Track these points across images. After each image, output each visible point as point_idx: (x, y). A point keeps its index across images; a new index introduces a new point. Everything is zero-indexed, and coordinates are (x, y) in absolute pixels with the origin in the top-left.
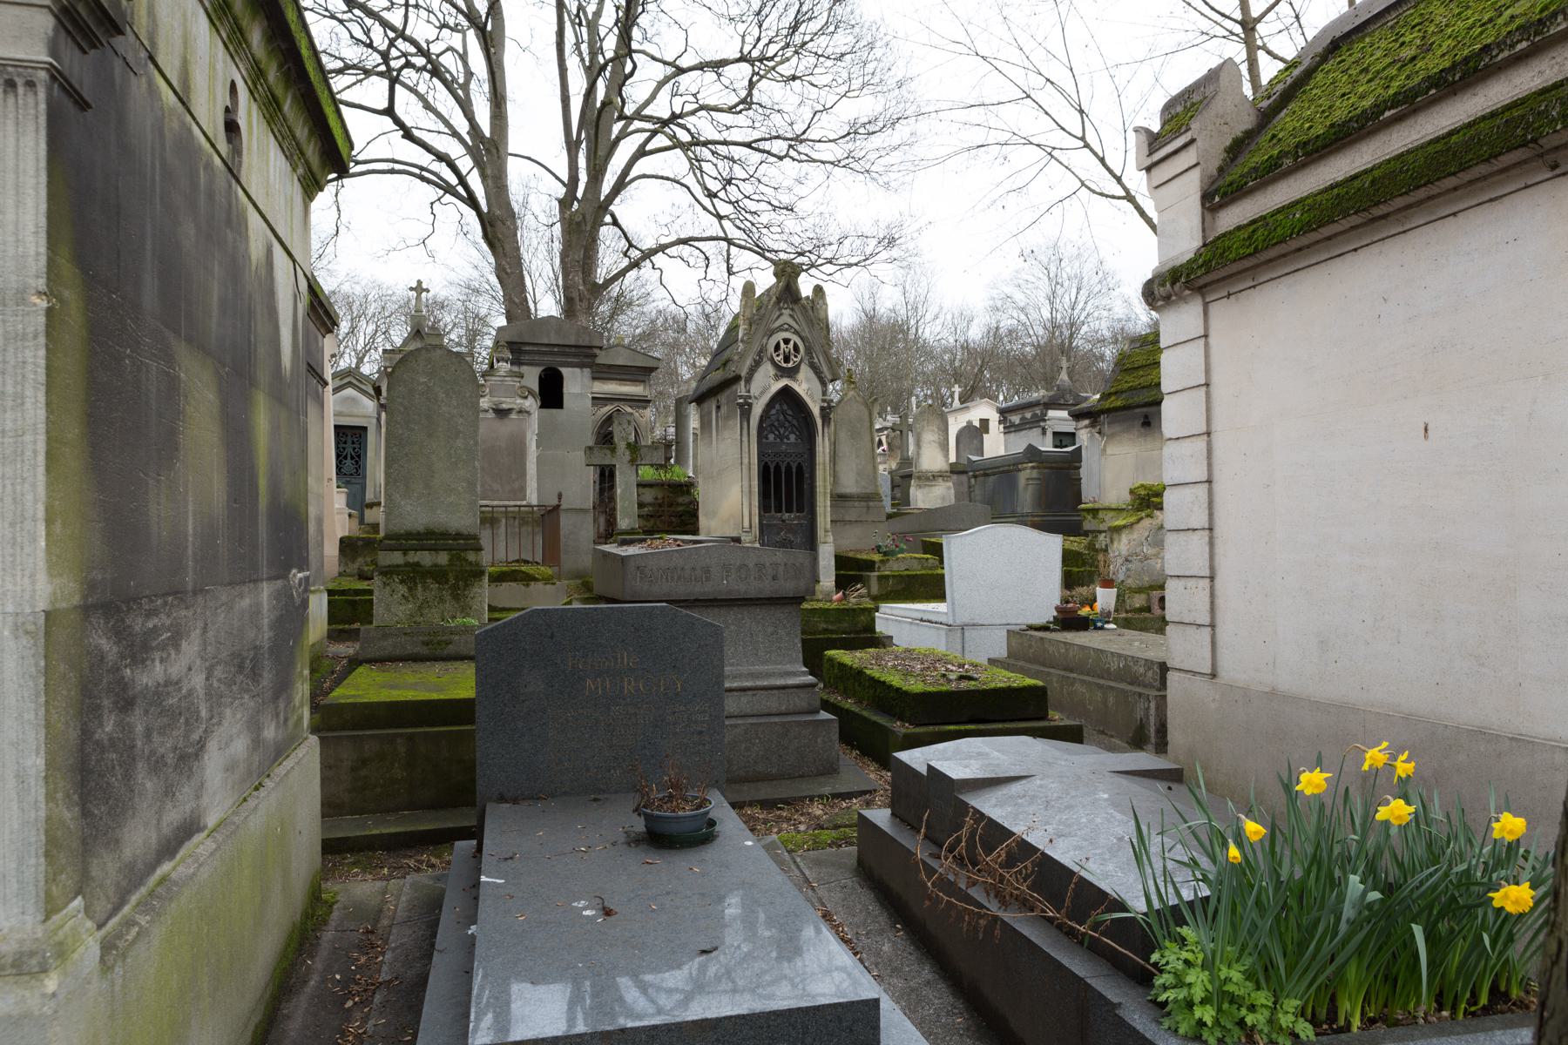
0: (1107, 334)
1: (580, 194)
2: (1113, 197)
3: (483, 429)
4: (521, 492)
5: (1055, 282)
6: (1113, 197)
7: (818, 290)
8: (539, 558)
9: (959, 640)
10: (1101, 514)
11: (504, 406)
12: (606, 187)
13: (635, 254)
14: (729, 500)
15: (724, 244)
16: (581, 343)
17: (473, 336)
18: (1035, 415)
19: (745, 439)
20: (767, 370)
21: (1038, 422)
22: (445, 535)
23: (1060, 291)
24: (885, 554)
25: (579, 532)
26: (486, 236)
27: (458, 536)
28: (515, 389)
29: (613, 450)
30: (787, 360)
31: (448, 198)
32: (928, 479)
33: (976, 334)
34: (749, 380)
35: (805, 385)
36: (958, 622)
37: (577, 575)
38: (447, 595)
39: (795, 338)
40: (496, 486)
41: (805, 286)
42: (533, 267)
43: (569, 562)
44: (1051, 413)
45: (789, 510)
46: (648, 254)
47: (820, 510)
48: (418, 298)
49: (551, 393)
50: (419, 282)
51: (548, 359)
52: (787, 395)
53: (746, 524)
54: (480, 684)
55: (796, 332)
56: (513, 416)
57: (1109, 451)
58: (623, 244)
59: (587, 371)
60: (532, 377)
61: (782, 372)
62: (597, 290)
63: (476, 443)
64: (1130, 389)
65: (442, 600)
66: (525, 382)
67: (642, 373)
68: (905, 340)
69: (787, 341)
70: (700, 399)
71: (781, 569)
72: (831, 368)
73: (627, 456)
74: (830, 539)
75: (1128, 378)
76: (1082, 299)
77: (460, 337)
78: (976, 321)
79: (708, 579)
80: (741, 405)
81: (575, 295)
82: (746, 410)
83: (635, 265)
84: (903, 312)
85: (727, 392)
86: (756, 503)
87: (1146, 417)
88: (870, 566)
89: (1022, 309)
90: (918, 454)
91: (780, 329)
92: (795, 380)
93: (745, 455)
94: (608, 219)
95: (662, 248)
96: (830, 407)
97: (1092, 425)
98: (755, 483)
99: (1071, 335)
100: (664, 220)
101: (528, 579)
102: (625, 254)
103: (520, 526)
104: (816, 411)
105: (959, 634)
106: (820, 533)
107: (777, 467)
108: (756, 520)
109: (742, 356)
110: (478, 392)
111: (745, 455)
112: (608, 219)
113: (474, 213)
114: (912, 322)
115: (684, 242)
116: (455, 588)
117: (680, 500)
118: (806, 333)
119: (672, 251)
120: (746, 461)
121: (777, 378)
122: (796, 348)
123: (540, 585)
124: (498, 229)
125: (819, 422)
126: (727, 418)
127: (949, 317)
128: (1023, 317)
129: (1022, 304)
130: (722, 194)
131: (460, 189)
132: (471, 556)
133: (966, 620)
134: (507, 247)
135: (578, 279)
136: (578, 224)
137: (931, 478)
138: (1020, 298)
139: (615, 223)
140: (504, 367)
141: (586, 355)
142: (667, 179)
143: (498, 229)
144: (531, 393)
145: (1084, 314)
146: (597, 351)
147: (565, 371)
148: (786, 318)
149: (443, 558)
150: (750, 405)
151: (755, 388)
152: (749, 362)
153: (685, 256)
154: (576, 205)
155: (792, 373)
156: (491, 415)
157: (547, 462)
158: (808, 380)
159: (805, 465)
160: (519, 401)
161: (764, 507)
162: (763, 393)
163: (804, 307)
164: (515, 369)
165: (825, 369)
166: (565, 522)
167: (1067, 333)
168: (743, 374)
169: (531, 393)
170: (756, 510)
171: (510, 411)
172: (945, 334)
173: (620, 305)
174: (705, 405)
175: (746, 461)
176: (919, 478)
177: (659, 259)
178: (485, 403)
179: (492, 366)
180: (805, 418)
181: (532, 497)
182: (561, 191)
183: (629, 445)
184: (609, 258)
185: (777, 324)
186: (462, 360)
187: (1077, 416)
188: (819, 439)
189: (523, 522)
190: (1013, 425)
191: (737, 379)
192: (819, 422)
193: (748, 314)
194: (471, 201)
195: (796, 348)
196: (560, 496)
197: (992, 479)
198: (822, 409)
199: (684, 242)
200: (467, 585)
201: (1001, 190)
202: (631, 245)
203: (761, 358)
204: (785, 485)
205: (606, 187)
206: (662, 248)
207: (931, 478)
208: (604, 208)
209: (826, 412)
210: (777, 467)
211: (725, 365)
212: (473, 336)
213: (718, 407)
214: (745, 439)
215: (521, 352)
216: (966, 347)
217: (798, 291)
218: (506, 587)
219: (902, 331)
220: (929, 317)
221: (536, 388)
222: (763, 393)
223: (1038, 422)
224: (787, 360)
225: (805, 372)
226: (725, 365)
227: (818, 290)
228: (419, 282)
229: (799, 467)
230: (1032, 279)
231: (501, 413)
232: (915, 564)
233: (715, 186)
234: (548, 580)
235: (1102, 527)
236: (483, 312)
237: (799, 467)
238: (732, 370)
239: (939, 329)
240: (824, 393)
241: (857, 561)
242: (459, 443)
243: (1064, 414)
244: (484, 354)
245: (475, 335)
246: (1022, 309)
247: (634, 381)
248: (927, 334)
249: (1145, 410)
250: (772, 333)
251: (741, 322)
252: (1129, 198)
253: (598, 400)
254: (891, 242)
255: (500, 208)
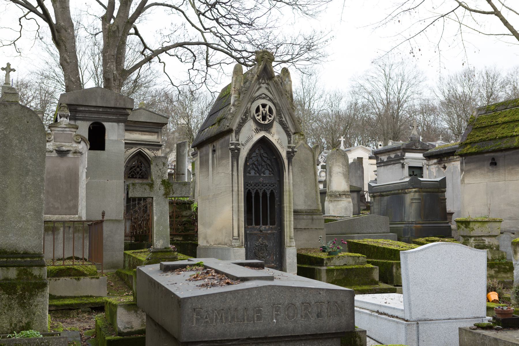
0: (418, 107)
1: (115, 14)
2: (484, 13)
3: (48, 164)
4: (74, 209)
5: (388, 77)
6: (484, 13)
7: (285, 71)
8: (86, 256)
9: (415, 332)
10: (471, 225)
11: (64, 148)
12: (132, 11)
13: (148, 52)
14: (221, 215)
15: (205, 47)
16: (118, 106)
17: (44, 104)
18: (397, 156)
19: (235, 173)
20: (250, 125)
21: (399, 160)
22: (15, 254)
23: (391, 82)
24: (330, 253)
25: (116, 236)
26: (54, 38)
27: (26, 254)
28: (73, 136)
29: (151, 185)
30: (264, 118)
31: (32, 15)
32: (336, 196)
33: (343, 107)
34: (238, 132)
35: (277, 137)
36: (414, 318)
37: (114, 266)
38: (15, 304)
39: (269, 104)
40: (57, 205)
41: (277, 70)
42: (82, 64)
43: (107, 257)
44: (407, 155)
45: (265, 224)
46: (156, 53)
47: (286, 223)
48: (7, 76)
49: (97, 139)
50: (9, 65)
51: (98, 113)
52: (264, 142)
53: (236, 234)
54: (46, 145)
55: (270, 100)
56: (70, 155)
57: (466, 181)
58: (142, 48)
59: (122, 125)
60: (84, 128)
61: (261, 127)
62: (125, 73)
63: (42, 180)
64: (481, 141)
65: (11, 308)
66: (79, 132)
67: (157, 127)
68: (303, 110)
69: (264, 106)
70: (199, 145)
71: (325, 307)
72: (294, 125)
73: (162, 191)
74: (294, 244)
75: (478, 134)
76: (404, 87)
77: (37, 104)
78: (343, 100)
79: (259, 318)
80: (232, 150)
81: (111, 77)
82: (235, 153)
83: (149, 59)
84: (301, 93)
85: (221, 141)
86: (242, 218)
87: (493, 159)
88: (320, 262)
89: (370, 93)
90: (330, 180)
91: (259, 97)
92: (270, 133)
93: (235, 185)
94: (132, 31)
95: (165, 50)
96: (293, 152)
97: (439, 163)
98: (242, 204)
99: (398, 108)
100: (166, 32)
101: (78, 274)
102: (142, 53)
103: (74, 233)
104: (284, 154)
105: (415, 327)
106: (287, 239)
107: (257, 193)
108: (242, 230)
109: (234, 115)
110: (45, 137)
111: (235, 185)
112: (132, 31)
113: (47, 24)
114: (307, 99)
115: (181, 45)
116: (22, 298)
117: (184, 213)
118: (277, 101)
119: (172, 51)
120: (235, 189)
121: (257, 131)
122: (270, 110)
123: (88, 279)
124: (62, 35)
125: (286, 162)
126: (221, 158)
127: (328, 97)
128: (371, 98)
129: (369, 90)
130: (208, 14)
131: (39, 10)
132: (36, 271)
133: (420, 317)
134: (68, 46)
135: (113, 67)
136: (114, 32)
137: (337, 196)
138: (368, 86)
139: (137, 33)
140: (64, 121)
141: (121, 113)
142: (170, 6)
143: (62, 35)
144: (83, 139)
145: (405, 96)
146: (129, 111)
147: (106, 125)
148: (263, 90)
149: (12, 273)
150: (239, 150)
151: (242, 138)
152: (238, 120)
153: (179, 54)
154: (112, 21)
155: (267, 128)
156: (54, 154)
157: (97, 190)
158: (278, 133)
159: (276, 192)
160: (75, 145)
161: (248, 221)
162: (247, 141)
163: (276, 82)
164: (72, 122)
165: (290, 125)
166: (106, 228)
167: (396, 107)
168: (234, 128)
169: (83, 139)
170: (242, 224)
171: (68, 151)
172: (326, 107)
173: (136, 84)
174: (204, 149)
175: (235, 189)
176: (331, 196)
177: (163, 56)
178: (50, 146)
179: (56, 120)
180: (276, 159)
181: (83, 214)
182: (102, 12)
183: (163, 182)
184: (131, 56)
185: (257, 94)
186: (35, 116)
187: (429, 157)
188: (286, 174)
189: (76, 230)
190: (382, 162)
191: (230, 131)
192: (286, 162)
193: (237, 87)
194: (46, 16)
195: (270, 110)
196: (103, 214)
197: (386, 198)
198: (288, 153)
199: (181, 45)
200: (31, 295)
201: (399, 10)
202: (146, 47)
203: (247, 117)
204: (262, 206)
205: (132, 11)
206: (165, 50)
207: (337, 196)
208: (130, 22)
209: (290, 155)
210: (257, 193)
211: (219, 121)
212: (44, 104)
213: (214, 151)
214: (235, 173)
215: (77, 111)
216: (338, 115)
217: (272, 72)
218: (63, 281)
219: (301, 105)
220: (316, 96)
221: (86, 136)
222: (247, 141)
223: (399, 160)
224: (264, 118)
225: (276, 127)
226: (219, 121)
227: (285, 71)
228: (9, 65)
229: (272, 193)
230: (375, 75)
231: (62, 153)
232: (351, 261)
233: (203, 8)
234: (93, 275)
235: (472, 234)
236: (51, 89)
237: (272, 193)
238: (225, 126)
239: (322, 103)
240: (289, 142)
241: (309, 258)
242: (29, 179)
243: (420, 155)
244: (51, 115)
245: (46, 104)
246: (370, 93)
247: (151, 132)
248: (315, 107)
249: (492, 154)
250: (254, 100)
251: (232, 92)
252: (497, 13)
253: (129, 145)
254: (309, 49)
255: (64, 21)
